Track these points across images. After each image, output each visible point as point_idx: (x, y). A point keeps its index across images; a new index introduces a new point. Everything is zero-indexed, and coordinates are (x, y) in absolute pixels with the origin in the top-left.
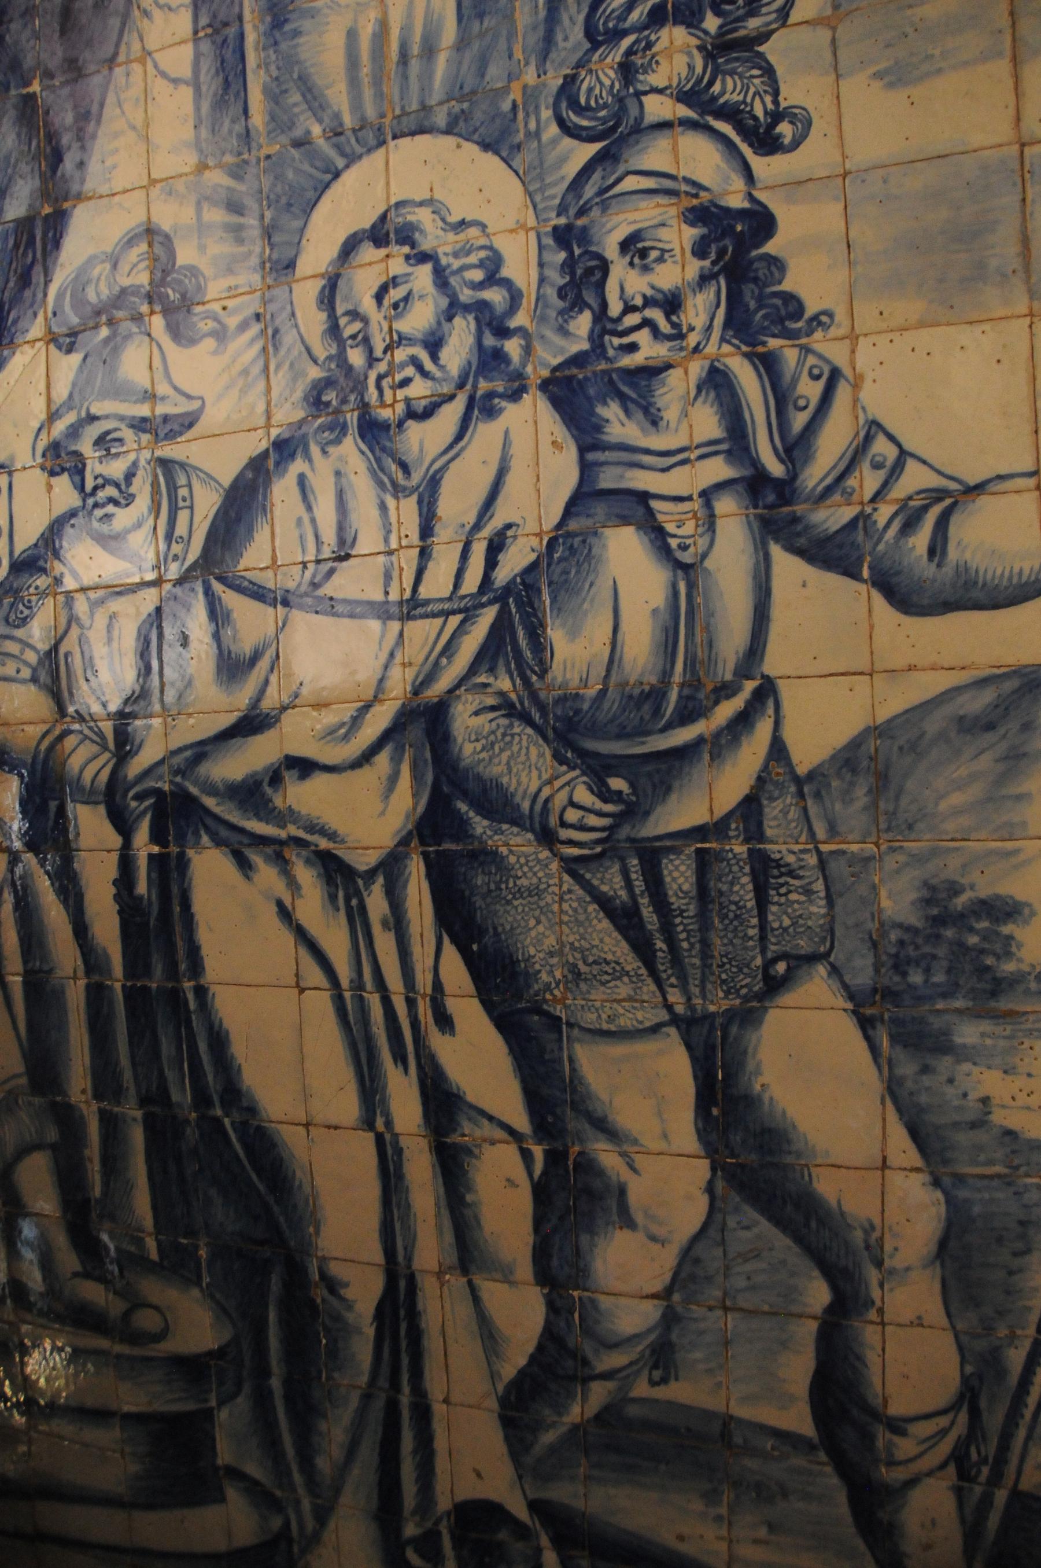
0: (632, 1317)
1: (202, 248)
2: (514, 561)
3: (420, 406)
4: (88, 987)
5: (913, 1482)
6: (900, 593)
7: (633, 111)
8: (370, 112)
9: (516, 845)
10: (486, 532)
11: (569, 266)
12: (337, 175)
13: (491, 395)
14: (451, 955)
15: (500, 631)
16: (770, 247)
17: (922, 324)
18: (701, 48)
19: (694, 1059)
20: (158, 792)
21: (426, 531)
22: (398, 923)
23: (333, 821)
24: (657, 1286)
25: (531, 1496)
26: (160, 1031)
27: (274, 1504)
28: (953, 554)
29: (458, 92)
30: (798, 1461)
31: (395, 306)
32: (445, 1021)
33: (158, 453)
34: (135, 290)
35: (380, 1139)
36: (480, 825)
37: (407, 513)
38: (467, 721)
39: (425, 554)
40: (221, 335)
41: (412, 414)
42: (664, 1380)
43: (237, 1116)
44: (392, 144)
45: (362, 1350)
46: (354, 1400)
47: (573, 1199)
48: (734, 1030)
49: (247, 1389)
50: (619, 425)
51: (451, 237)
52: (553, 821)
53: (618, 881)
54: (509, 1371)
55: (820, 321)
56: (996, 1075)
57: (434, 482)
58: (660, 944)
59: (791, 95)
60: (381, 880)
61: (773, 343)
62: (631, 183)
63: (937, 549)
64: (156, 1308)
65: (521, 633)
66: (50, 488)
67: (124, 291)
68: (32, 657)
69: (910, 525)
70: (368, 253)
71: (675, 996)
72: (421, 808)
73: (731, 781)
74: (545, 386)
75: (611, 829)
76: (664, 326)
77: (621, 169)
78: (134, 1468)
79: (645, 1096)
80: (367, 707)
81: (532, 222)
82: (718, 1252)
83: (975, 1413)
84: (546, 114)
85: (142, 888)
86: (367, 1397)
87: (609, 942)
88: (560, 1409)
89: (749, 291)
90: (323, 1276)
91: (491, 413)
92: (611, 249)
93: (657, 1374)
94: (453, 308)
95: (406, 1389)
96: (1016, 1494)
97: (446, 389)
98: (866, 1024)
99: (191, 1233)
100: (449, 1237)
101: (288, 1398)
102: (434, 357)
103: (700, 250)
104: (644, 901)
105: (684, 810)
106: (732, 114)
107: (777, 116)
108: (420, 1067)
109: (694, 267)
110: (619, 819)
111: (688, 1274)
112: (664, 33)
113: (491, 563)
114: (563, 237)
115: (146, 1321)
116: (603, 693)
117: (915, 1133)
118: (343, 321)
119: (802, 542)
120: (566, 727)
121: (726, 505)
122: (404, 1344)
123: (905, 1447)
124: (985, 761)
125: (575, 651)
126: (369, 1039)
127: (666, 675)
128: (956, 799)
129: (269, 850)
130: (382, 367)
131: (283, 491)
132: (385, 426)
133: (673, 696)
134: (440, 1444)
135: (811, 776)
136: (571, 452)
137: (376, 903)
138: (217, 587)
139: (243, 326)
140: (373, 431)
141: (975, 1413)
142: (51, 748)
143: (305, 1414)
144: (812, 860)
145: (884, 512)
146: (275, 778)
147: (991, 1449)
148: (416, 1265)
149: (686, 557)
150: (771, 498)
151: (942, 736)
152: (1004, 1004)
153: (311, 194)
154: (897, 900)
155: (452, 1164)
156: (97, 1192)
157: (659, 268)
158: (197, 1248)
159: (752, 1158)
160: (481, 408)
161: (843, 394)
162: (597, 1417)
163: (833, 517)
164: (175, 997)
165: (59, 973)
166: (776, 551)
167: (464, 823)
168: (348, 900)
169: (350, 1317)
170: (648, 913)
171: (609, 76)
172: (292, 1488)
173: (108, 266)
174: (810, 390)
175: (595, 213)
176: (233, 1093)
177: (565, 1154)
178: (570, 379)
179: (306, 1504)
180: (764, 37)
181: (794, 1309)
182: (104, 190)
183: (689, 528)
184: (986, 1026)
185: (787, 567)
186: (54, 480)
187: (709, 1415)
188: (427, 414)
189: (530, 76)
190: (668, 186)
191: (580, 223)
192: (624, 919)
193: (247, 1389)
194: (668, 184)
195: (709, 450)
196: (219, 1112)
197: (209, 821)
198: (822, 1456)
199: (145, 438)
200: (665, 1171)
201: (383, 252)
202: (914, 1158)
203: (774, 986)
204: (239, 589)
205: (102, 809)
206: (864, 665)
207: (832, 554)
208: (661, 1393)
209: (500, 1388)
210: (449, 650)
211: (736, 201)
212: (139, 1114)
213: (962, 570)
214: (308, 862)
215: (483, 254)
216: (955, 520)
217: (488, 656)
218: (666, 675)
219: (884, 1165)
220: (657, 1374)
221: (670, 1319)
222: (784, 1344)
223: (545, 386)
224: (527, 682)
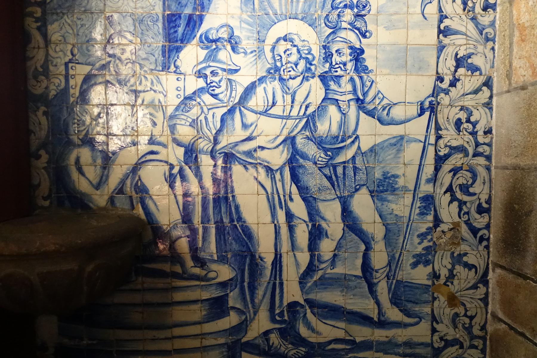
1: (241, 32)
2: (310, 110)
3: (292, 77)
4: (202, 197)
6: (381, 121)
7: (340, 25)
9: (309, 164)
10: (306, 104)
11: (325, 53)
12: (275, 23)
13: (308, 77)
14: (294, 186)
16: (363, 56)
17: (389, 74)
18: (353, 15)
19: (341, 205)
23: (268, 159)
24: (333, 249)
27: (243, 313)
29: (304, 12)
30: (359, 281)
31: (288, 55)
32: (291, 199)
33: (228, 77)
35: (275, 225)
36: (301, 161)
37: (289, 98)
38: (300, 141)
40: (245, 53)
41: (291, 78)
43: (240, 223)
44: (288, 19)
46: (266, 284)
48: (349, 199)
49: (238, 286)
50: (333, 86)
51: (301, 43)
53: (328, 171)
54: (302, 271)
55: (371, 71)
56: (394, 205)
57: (295, 92)
58: (336, 183)
60: (279, 171)
61: (363, 74)
62: (338, 39)
64: (215, 271)
65: (311, 124)
66: (197, 81)
67: (220, 38)
69: (384, 110)
70: (282, 42)
71: (338, 193)
72: (289, 157)
73: (350, 153)
74: (319, 76)
75: (327, 161)
76: (343, 68)
77: (336, 36)
78: (204, 313)
79: (331, 211)
81: (318, 43)
82: (344, 241)
83: (390, 267)
84: (322, 21)
87: (327, 183)
89: (359, 64)
90: (260, 257)
91: (308, 80)
92: (334, 52)
93: (332, 268)
94: (301, 57)
95: (278, 279)
96: (397, 281)
97: (299, 74)
98: (372, 196)
99: (226, 252)
100: (290, 244)
101: (249, 287)
102: (296, 67)
104: (333, 175)
105: (340, 159)
106: (358, 29)
107: (366, 31)
108: (286, 209)
109: (349, 58)
111: (339, 246)
112: (347, 10)
113: (306, 110)
114: (325, 47)
115: (212, 275)
116: (327, 136)
118: (276, 56)
119: (365, 111)
121: (352, 103)
122: (278, 269)
123: (378, 275)
124: (394, 151)
125: (322, 128)
126: (274, 204)
127: (339, 133)
128: (389, 157)
129: (253, 165)
130: (284, 67)
131: (260, 90)
133: (340, 137)
135: (364, 153)
137: (278, 176)
138: (242, 108)
140: (281, 80)
141: (390, 267)
142: (195, 142)
143: (253, 288)
144: (364, 168)
146: (255, 150)
147: (393, 273)
148: (282, 252)
149: (344, 112)
150: (360, 103)
151: (387, 147)
152: (396, 192)
153: (269, 26)
154: (378, 174)
155: (291, 229)
156: (200, 245)
157: (343, 57)
158: (227, 255)
159: (351, 223)
160: (305, 79)
161: (374, 84)
162: (319, 279)
163: (371, 107)
164: (226, 198)
166: (361, 112)
167: (298, 160)
168: (271, 175)
169: (266, 265)
170: (334, 177)
171: (335, 16)
172: (249, 308)
173: (216, 31)
174: (368, 84)
175: (331, 43)
177: (315, 225)
178: (324, 76)
179: (252, 311)
180: (365, 15)
181: (358, 251)
182: (215, 12)
183: (345, 107)
184: (393, 196)
185: (362, 115)
186: (198, 79)
188: (294, 79)
189: (319, 12)
191: (328, 45)
192: (329, 178)
193: (238, 286)
194: (345, 41)
195: (350, 92)
196: (236, 223)
197: (238, 159)
198: (363, 279)
199: (225, 73)
200: (334, 225)
201: (286, 43)
202: (380, 220)
203: (357, 190)
204: (246, 109)
205: (209, 156)
206: (374, 133)
207: (371, 114)
208: (333, 271)
209: (299, 275)
210: (296, 126)
212: (214, 226)
213: (392, 118)
214: (262, 168)
215: (308, 48)
218: (339, 133)
220: (332, 268)
221: (335, 256)
222: (356, 258)
223: (319, 76)
224: (312, 133)
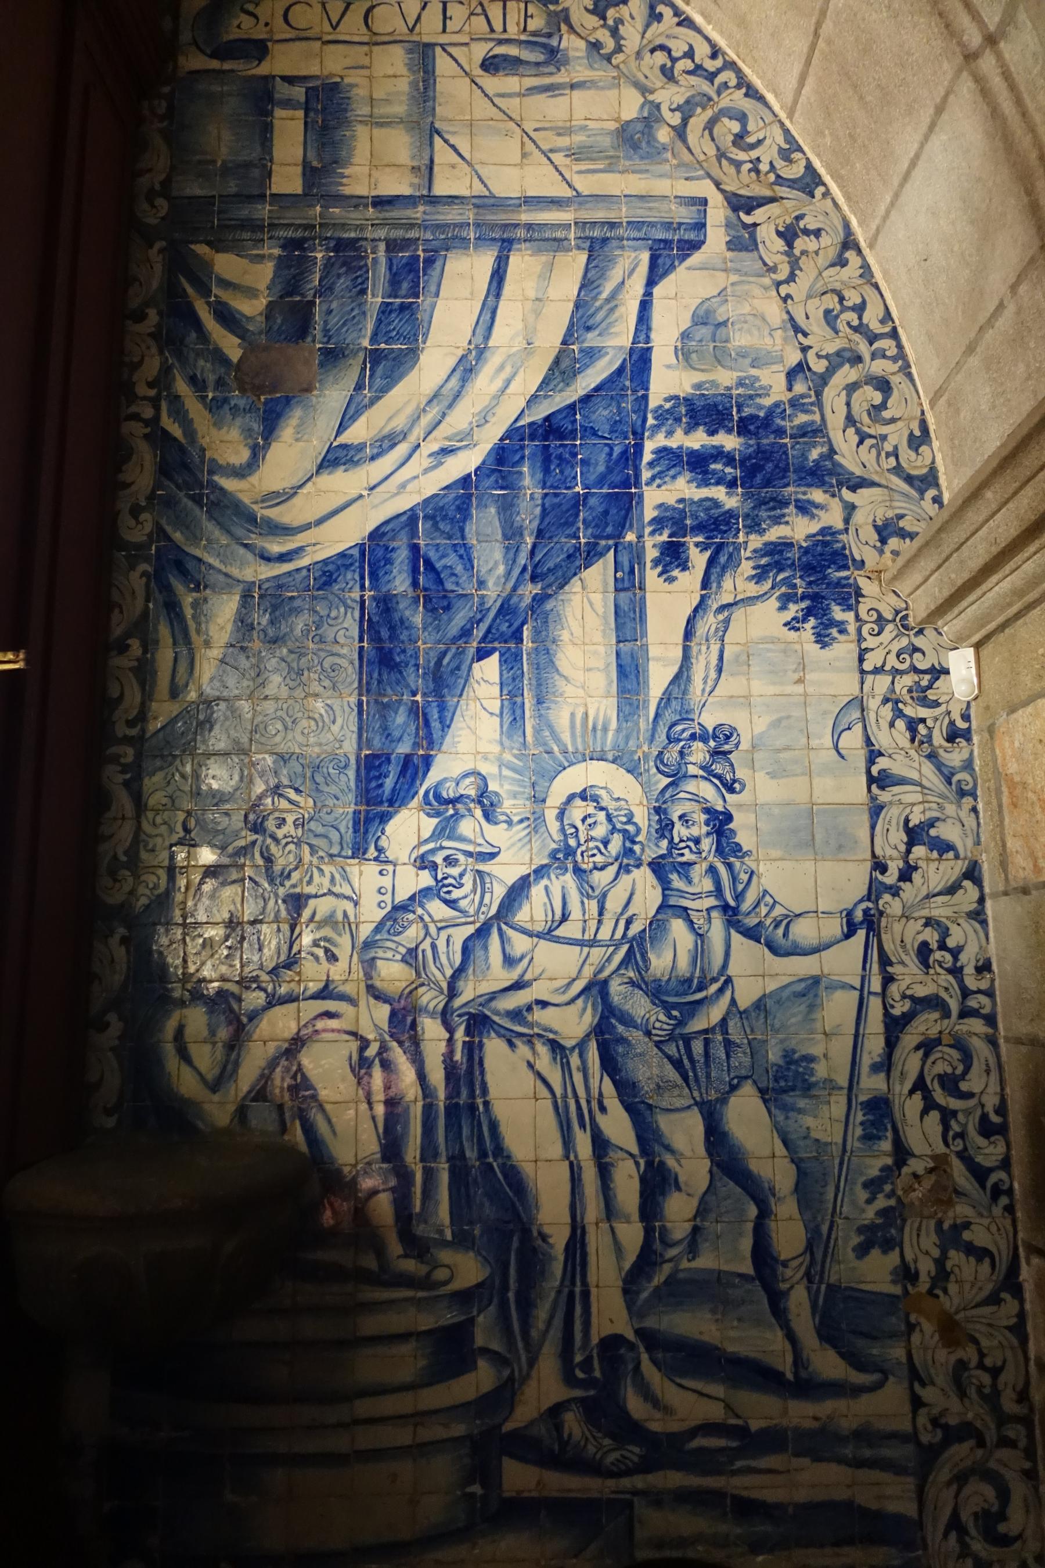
0: (680, 1230)
1: (502, 786)
2: (635, 929)
3: (599, 866)
4: (424, 1106)
5: (792, 1287)
6: (773, 949)
7: (684, 769)
8: (580, 748)
9: (636, 1036)
10: (626, 916)
11: (660, 821)
13: (628, 865)
15: (630, 952)
16: (731, 826)
19: (704, 1119)
20: (469, 1013)
21: (601, 913)
22: (584, 1070)
23: (556, 1027)
24: (691, 1216)
25: (636, 1326)
26: (463, 1122)
28: (791, 937)
29: (616, 747)
32: (603, 1109)
34: (468, 797)
35: (571, 1164)
36: (620, 1028)
37: (593, 906)
38: (616, 988)
39: (600, 922)
40: (510, 823)
41: (595, 868)
42: (694, 1258)
43: (500, 1160)
45: (557, 1268)
46: (553, 1294)
47: (657, 1182)
49: (495, 1300)
50: (677, 882)
52: (650, 1027)
53: (675, 1049)
54: (627, 1265)
55: (748, 853)
57: (604, 895)
59: (739, 775)
62: (682, 795)
63: (785, 934)
65: (638, 956)
68: (403, 951)
69: (776, 926)
70: (578, 802)
71: (696, 1094)
73: (716, 1013)
74: (650, 864)
79: (684, 1133)
80: (574, 980)
83: (812, 1254)
84: (652, 764)
85: (458, 1056)
86: (559, 1292)
88: (650, 1279)
91: (628, 872)
92: (675, 818)
94: (614, 830)
95: (578, 1283)
96: (829, 1286)
99: (471, 1223)
100: (602, 1205)
101: (518, 1302)
102: (606, 847)
103: (707, 824)
104: (685, 1057)
105: (698, 1024)
106: (719, 777)
107: (734, 781)
108: (592, 1130)
109: (705, 829)
110: (676, 1026)
111: (702, 1211)
113: (627, 928)
114: (658, 810)
115: (441, 1274)
117: (785, 1143)
120: (656, 991)
121: (715, 914)
123: (789, 1272)
125: (660, 963)
128: (793, 1020)
130: (583, 848)
131: (537, 891)
132: (585, 872)
134: (594, 1310)
136: (659, 890)
137: (575, 1060)
138: (504, 927)
139: (521, 821)
140: (578, 871)
141: (812, 1254)
142: (411, 992)
143: (526, 1306)
145: (768, 922)
146: (529, 1009)
147: (819, 1268)
149: (700, 932)
151: (788, 998)
154: (774, 1055)
155: (604, 1171)
156: (417, 1209)
161: (755, 878)
162: (665, 1282)
163: (751, 921)
164: (472, 1108)
165: (407, 1099)
166: (732, 931)
167: (614, 1027)
169: (553, 1252)
170: (686, 1061)
171: (675, 755)
174: (744, 877)
176: (499, 1150)
179: (524, 1358)
180: (731, 752)
183: (702, 921)
184: (807, 1101)
185: (736, 937)
187: (711, 1271)
188: (602, 869)
189: (645, 748)
190: (696, 799)
192: (677, 1064)
193: (495, 1300)
196: (491, 1160)
198: (757, 1283)
199: (470, 860)
200: (692, 1165)
202: (784, 1152)
203: (733, 1088)
205: (439, 1021)
207: (752, 934)
210: (609, 960)
211: (720, 808)
212: (446, 1166)
213: (794, 942)
216: (792, 925)
217: (625, 962)
219: (774, 1156)
223: (650, 864)
